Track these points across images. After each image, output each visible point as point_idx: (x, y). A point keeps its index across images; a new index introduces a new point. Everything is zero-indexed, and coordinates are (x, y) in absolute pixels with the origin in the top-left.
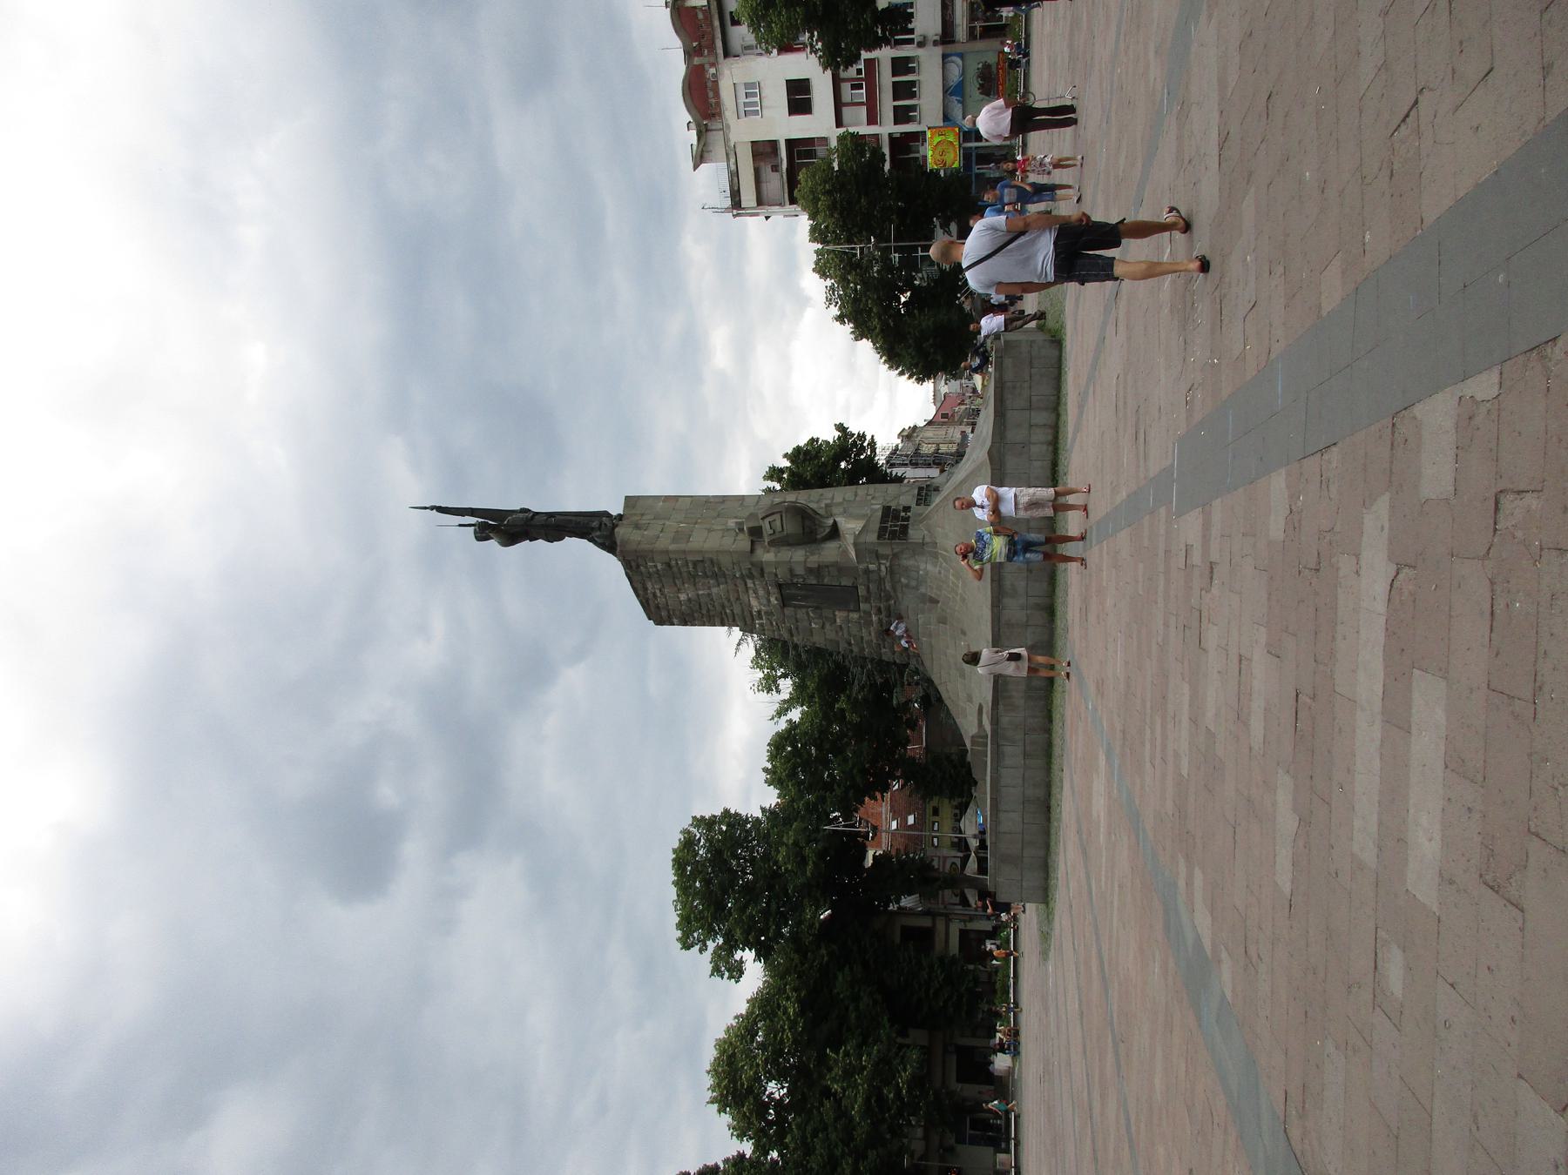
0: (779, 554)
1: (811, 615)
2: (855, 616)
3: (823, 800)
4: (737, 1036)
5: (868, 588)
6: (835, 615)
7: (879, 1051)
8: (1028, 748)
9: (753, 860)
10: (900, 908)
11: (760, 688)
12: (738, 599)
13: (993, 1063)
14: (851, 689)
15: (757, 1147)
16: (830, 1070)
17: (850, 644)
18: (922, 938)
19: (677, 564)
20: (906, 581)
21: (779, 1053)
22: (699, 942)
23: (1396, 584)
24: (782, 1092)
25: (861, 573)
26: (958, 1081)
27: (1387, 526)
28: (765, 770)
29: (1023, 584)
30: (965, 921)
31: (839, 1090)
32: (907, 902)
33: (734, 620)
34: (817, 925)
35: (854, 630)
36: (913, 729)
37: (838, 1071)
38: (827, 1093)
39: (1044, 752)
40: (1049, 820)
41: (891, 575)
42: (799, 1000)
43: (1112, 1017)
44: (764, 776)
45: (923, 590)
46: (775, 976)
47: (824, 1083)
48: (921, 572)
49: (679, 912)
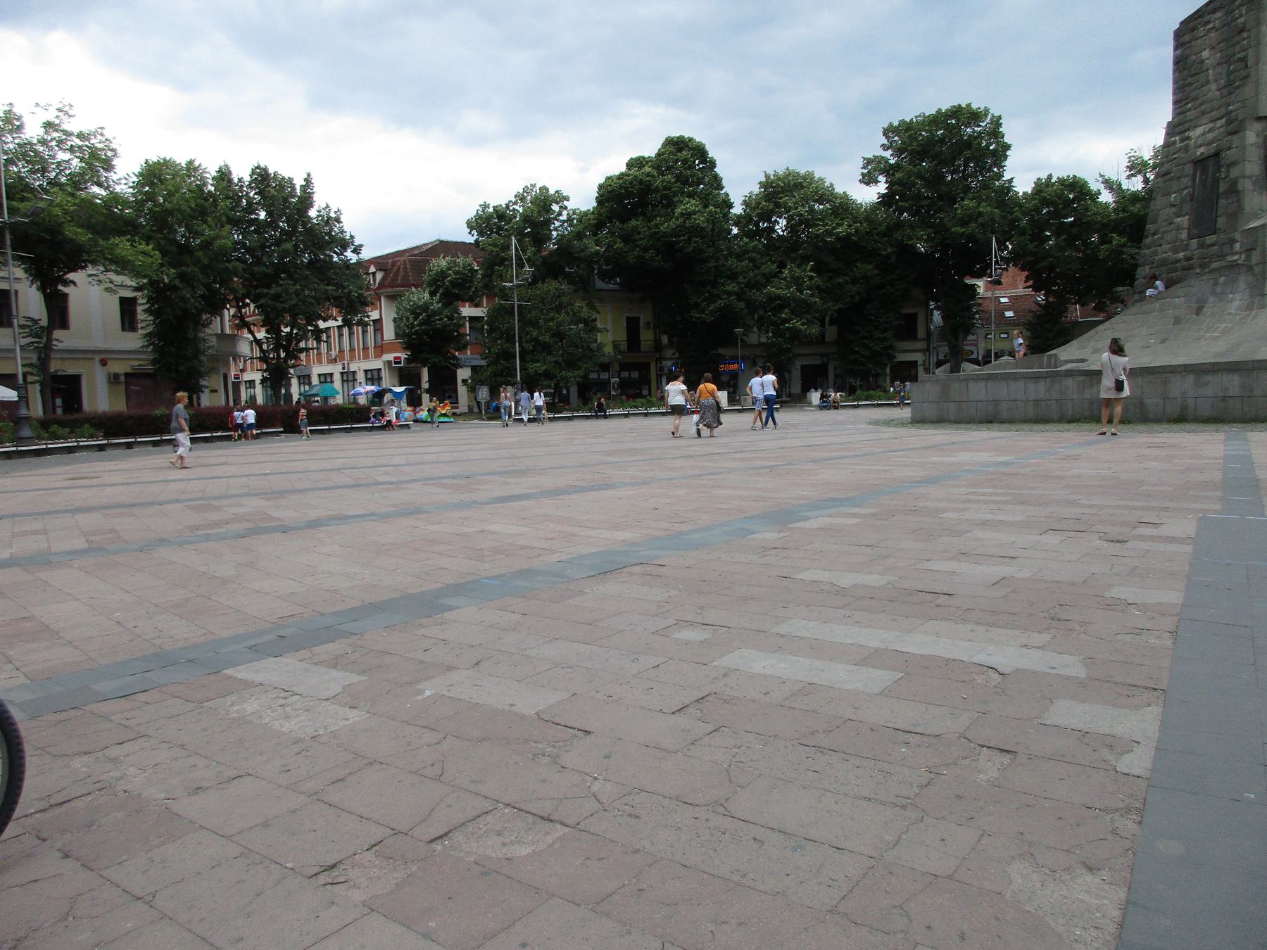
0: (1254, 148)
1: (1185, 192)
2: (1184, 235)
3: (1022, 234)
4: (817, 187)
5: (1215, 245)
6: (1184, 216)
7: (815, 302)
8: (1043, 403)
9: (965, 178)
10: (932, 310)
11: (1132, 159)
12: (1203, 113)
13: (816, 391)
14: (1131, 247)
15: (739, 217)
16: (799, 266)
17: (1154, 234)
18: (908, 331)
19: (1244, 39)
20: (1221, 282)
21: (808, 224)
22: (891, 143)
23: (991, 672)
24: (779, 231)
25: (1230, 236)
26: (803, 367)
27: (1054, 672)
28: (1050, 177)
29: (1210, 394)
30: (924, 364)
31: (784, 275)
32: (937, 316)
33: (1179, 114)
34: (911, 242)
35: (1168, 237)
36: (1095, 308)
37: (798, 272)
38: (782, 265)
39: (1040, 417)
40: (981, 422)
41: (1228, 266)
42: (848, 236)
43: (795, 464)
44: (1044, 176)
45: (1211, 299)
46: (867, 212)
47: (788, 262)
48: (1231, 296)
49: (914, 120)
